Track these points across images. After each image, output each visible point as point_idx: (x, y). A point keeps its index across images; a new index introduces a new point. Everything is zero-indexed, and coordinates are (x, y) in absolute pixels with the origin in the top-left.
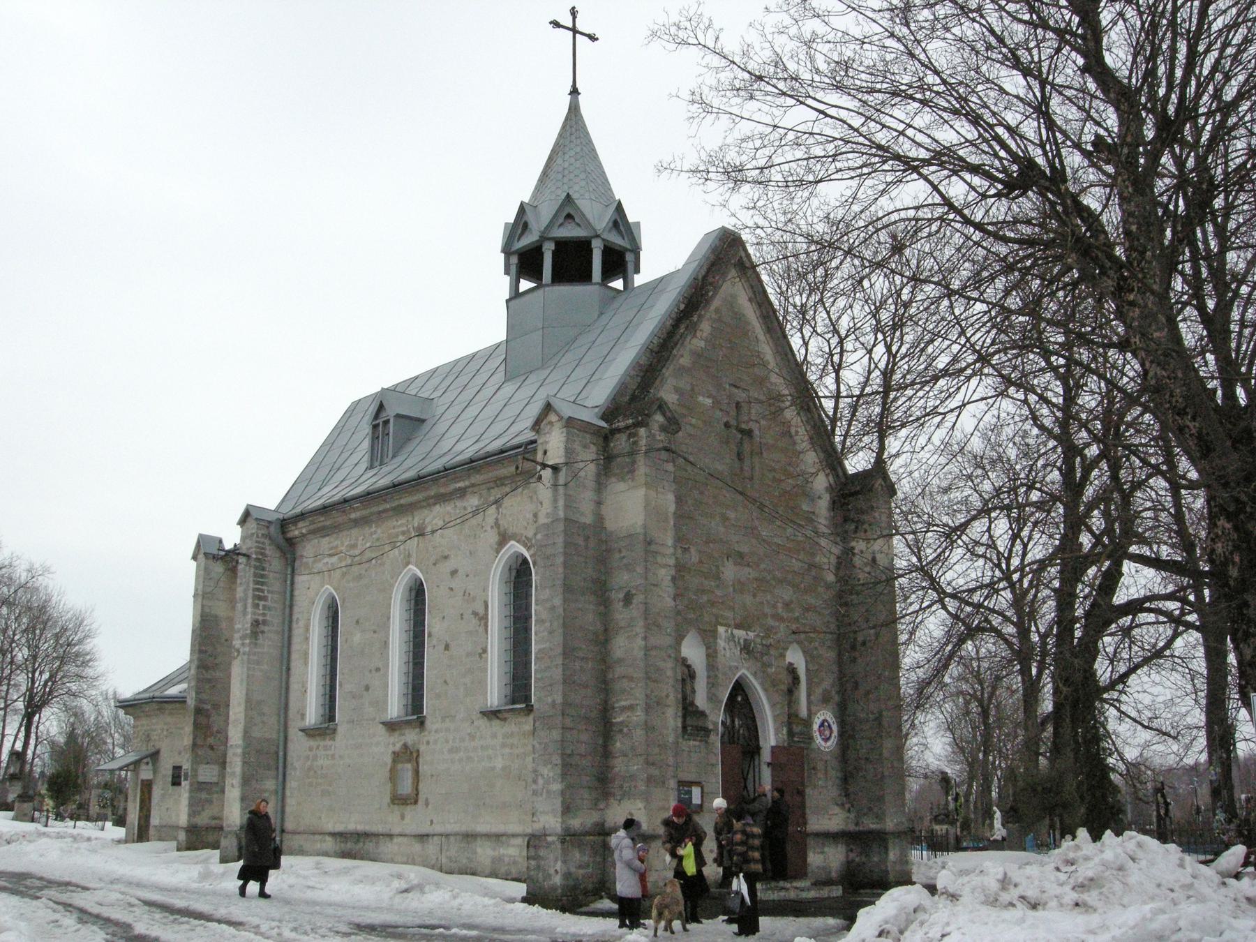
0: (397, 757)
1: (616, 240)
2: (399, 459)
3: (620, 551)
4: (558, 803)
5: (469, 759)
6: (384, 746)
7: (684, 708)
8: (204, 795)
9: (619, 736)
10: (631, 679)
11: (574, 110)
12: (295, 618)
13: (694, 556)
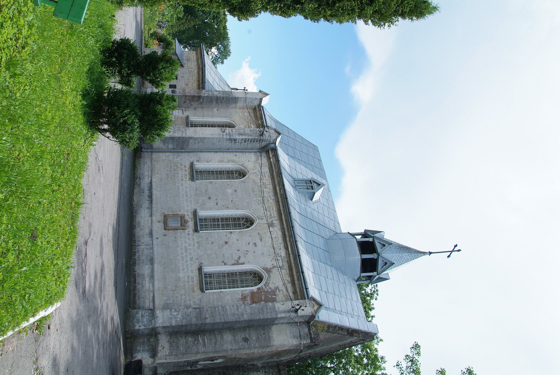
0: (182, 217)
3: (264, 334)
4: (167, 324)
5: (183, 258)
9: (194, 340)
10: (215, 344)
11: (424, 253)
12: (237, 154)
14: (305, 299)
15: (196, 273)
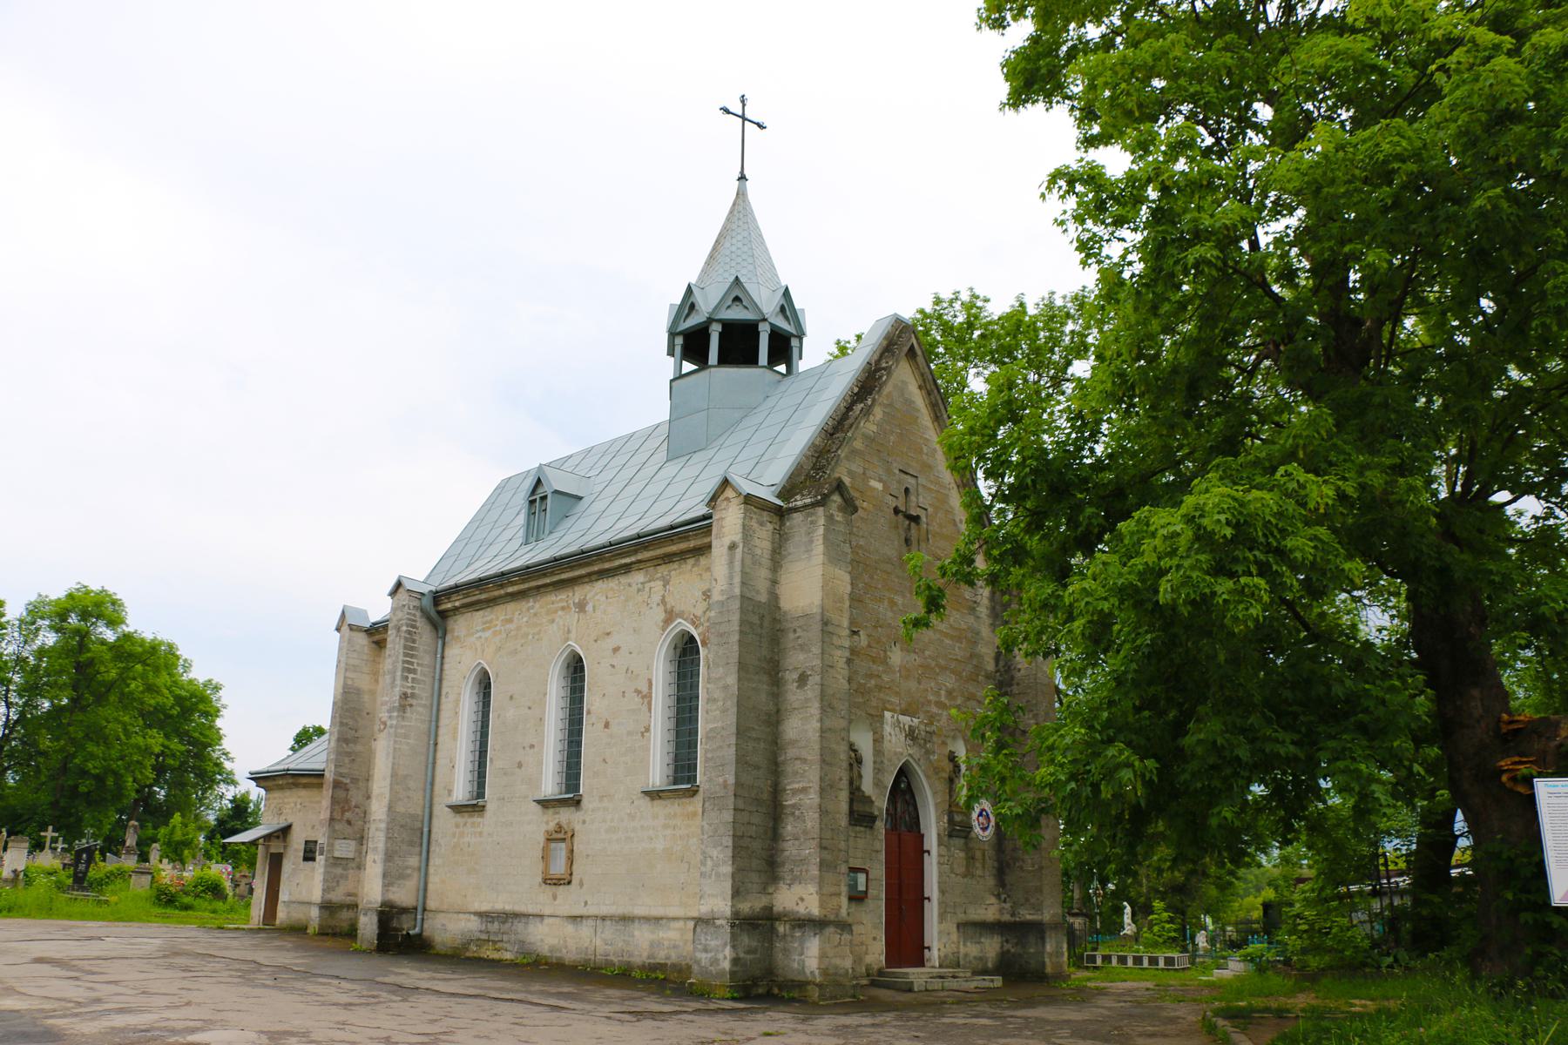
1: (781, 323)
2: (556, 535)
4: (728, 885)
6: (538, 824)
7: (851, 793)
8: (339, 871)
10: (804, 761)
11: (741, 194)
12: (444, 692)
13: (863, 640)
14: (710, 525)
15: (659, 807)
